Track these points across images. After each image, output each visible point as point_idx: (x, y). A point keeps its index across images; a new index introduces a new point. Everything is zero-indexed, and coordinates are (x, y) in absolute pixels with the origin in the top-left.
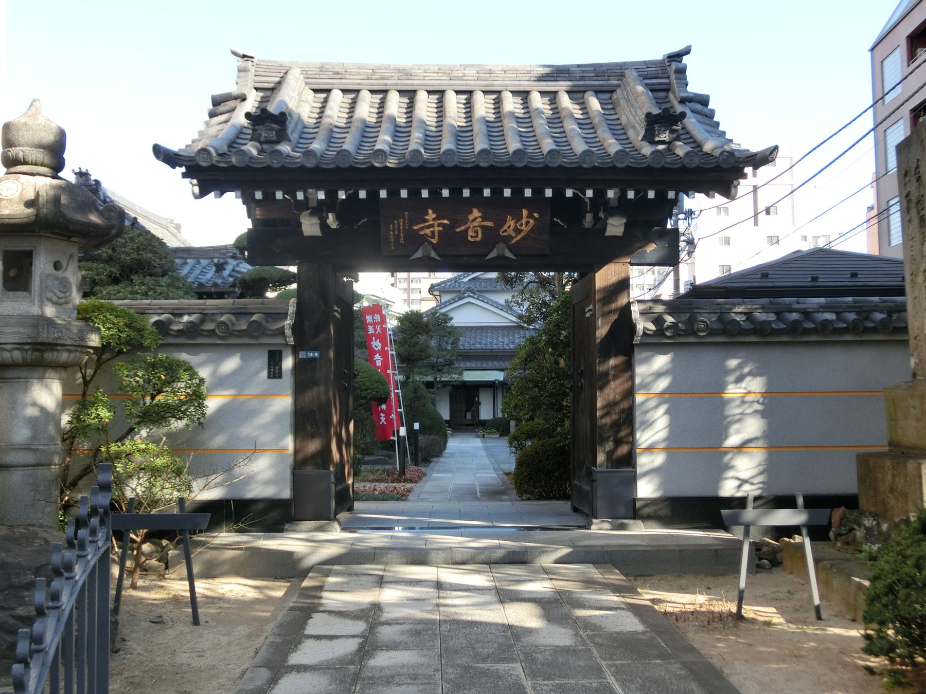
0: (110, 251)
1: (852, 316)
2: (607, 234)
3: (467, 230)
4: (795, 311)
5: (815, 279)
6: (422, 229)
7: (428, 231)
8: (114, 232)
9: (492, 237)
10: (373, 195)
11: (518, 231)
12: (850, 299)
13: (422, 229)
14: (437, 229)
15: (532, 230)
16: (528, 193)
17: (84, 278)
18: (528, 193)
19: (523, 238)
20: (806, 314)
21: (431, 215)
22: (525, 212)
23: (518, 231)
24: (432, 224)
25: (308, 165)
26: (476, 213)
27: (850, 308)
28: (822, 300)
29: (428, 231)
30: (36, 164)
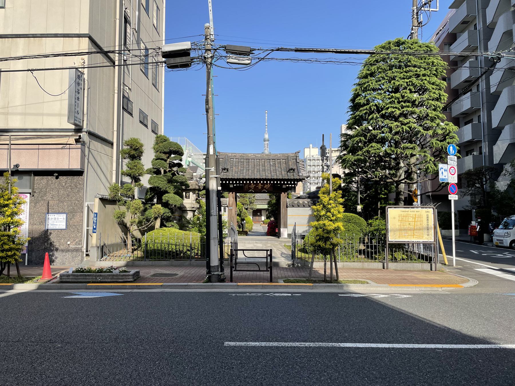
9: (263, 188)
24: (253, 186)
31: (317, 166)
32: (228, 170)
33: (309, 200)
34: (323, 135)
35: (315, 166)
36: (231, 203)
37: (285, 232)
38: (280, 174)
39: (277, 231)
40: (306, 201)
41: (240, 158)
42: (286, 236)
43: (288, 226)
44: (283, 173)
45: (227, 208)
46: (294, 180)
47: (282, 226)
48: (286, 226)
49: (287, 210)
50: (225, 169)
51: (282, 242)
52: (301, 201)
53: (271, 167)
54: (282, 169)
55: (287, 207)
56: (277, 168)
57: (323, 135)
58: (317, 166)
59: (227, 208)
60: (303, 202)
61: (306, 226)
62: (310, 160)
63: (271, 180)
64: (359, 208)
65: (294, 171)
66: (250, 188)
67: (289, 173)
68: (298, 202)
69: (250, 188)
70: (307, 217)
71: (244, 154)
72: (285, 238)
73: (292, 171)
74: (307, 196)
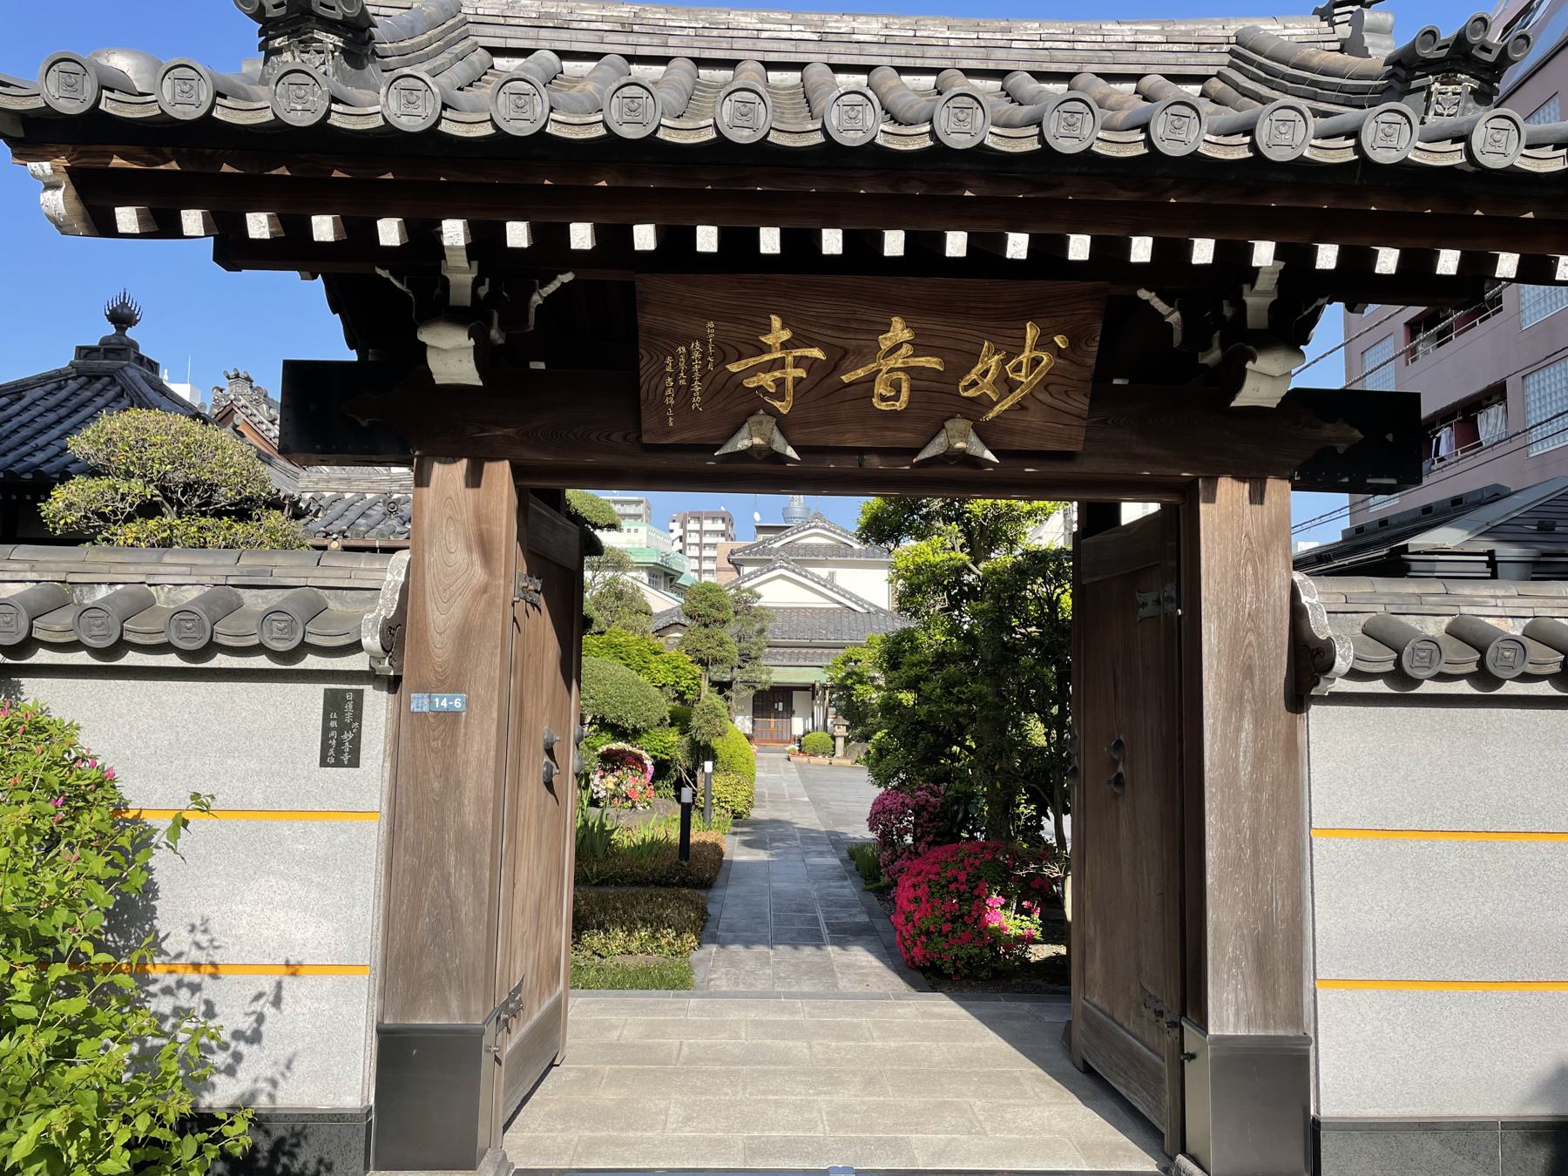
3: (871, 379)
6: (752, 371)
7: (767, 380)
11: (1007, 385)
13: (752, 371)
15: (1045, 385)
19: (1021, 406)
22: (1031, 332)
23: (1007, 385)
29: (767, 380)
36: (440, 619)
41: (617, 45)
45: (377, 705)
49: (1293, 751)
55: (1299, 696)
59: (377, 705)
66: (744, 405)
69: (744, 405)
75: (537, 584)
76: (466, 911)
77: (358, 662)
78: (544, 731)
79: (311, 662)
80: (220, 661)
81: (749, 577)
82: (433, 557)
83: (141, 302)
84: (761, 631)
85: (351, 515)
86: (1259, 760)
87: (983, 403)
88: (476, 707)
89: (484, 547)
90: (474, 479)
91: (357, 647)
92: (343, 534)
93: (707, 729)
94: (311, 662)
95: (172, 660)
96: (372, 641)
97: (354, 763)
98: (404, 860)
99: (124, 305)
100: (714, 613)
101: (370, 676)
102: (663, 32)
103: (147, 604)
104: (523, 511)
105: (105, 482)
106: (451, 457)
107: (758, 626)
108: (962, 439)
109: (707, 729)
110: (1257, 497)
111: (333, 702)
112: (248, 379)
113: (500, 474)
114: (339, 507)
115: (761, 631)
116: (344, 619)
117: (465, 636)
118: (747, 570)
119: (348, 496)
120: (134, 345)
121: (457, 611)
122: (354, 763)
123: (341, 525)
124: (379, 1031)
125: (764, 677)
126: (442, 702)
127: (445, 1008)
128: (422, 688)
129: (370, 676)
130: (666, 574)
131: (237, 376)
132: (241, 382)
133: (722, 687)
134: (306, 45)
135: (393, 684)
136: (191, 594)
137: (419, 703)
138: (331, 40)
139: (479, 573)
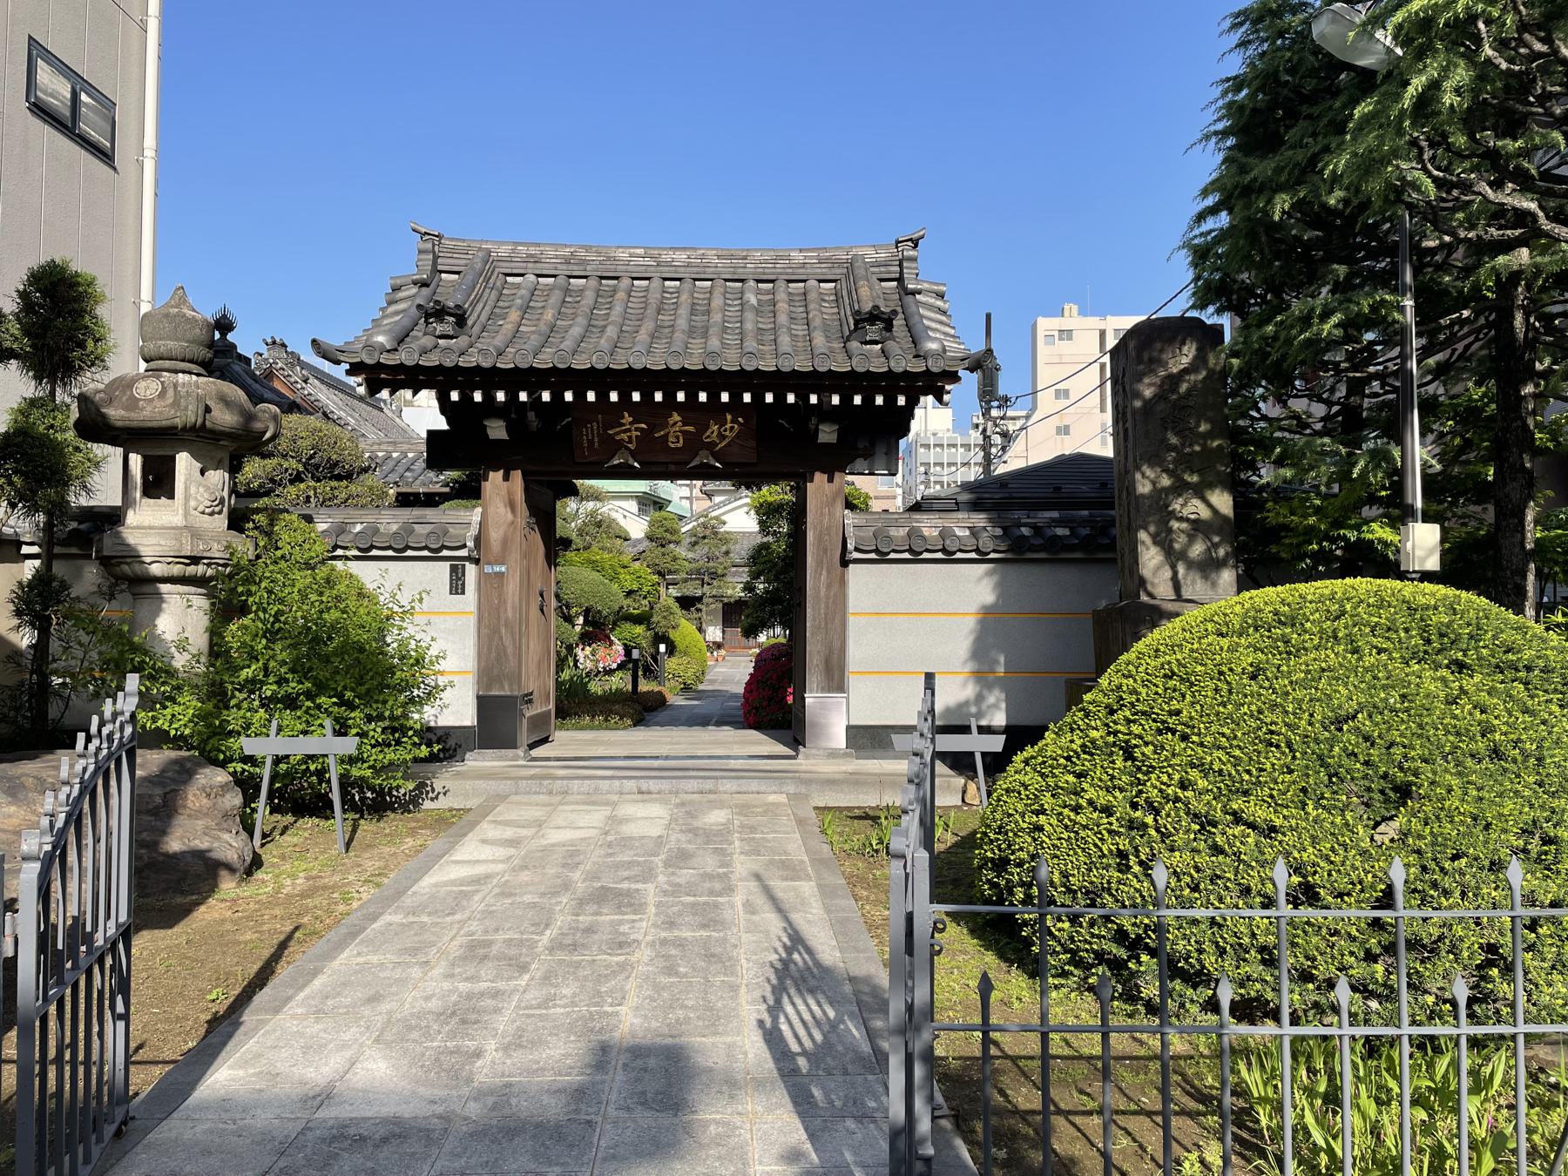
0: (1376, 837)
1: (1084, 531)
2: (1108, 452)
3: (667, 435)
4: (1025, 525)
5: (1058, 489)
6: (618, 433)
7: (625, 436)
8: (268, 435)
9: (694, 443)
10: (489, 397)
11: (722, 437)
12: (1086, 513)
13: (618, 433)
14: (635, 433)
15: (737, 436)
16: (681, 396)
17: (97, 361)
18: (681, 396)
19: (729, 445)
20: (1037, 529)
21: (627, 418)
22: (729, 417)
23: (722, 437)
24: (629, 430)
25: (484, 365)
26: (676, 417)
27: (1084, 522)
28: (1055, 514)
29: (625, 436)
30: (183, 360)
31: (949, 465)
32: (461, 320)
33: (979, 519)
34: (988, 317)
35: (942, 465)
36: (495, 536)
37: (832, 716)
38: (806, 342)
39: (790, 700)
40: (962, 525)
41: (563, 270)
42: (839, 739)
43: (853, 682)
44: (819, 340)
45: (471, 570)
46: (892, 382)
47: (813, 678)
48: (836, 681)
49: (843, 582)
50: (439, 313)
51: (809, 780)
52: (929, 526)
53: (749, 315)
54: (817, 322)
55: (845, 563)
56: (783, 319)
57: (988, 317)
58: (949, 465)
59: (471, 570)
60: (945, 534)
61: (960, 678)
62: (927, 446)
63: (739, 380)
64: (1423, 542)
65: (889, 326)
66: (616, 446)
67: (854, 345)
68: (914, 533)
69: (616, 446)
70: (969, 624)
71: (588, 248)
72: (833, 754)
73: (873, 331)
74: (965, 497)
75: (533, 520)
76: (510, 650)
77: (463, 553)
78: (539, 586)
79: (445, 553)
80: (409, 553)
81: (719, 506)
82: (491, 510)
83: (236, 314)
84: (727, 553)
85: (400, 469)
86: (829, 586)
87: (714, 444)
88: (511, 571)
89: (512, 505)
90: (506, 478)
91: (464, 546)
92: (396, 483)
93: (664, 623)
94: (445, 553)
95: (390, 553)
96: (470, 544)
97: (463, 593)
98: (485, 631)
99: (224, 316)
100: (669, 536)
101: (469, 559)
102: (583, 262)
103: (377, 531)
104: (527, 489)
105: (275, 461)
106: (496, 470)
107: (724, 548)
108: (705, 458)
109: (664, 623)
110: (831, 480)
111: (454, 569)
112: (284, 345)
113: (517, 476)
114: (391, 464)
115: (727, 553)
116: (456, 536)
117: (505, 543)
118: (717, 499)
119: (395, 455)
120: (234, 346)
121: (501, 532)
122: (463, 593)
123: (393, 477)
124: (479, 698)
125: (730, 592)
126: (497, 569)
127: (502, 688)
128: (489, 563)
129: (469, 559)
130: (655, 503)
131: (274, 343)
132: (277, 348)
133: (687, 603)
134: (442, 321)
135: (477, 562)
136: (394, 527)
137: (488, 569)
138: (452, 319)
139: (510, 516)
